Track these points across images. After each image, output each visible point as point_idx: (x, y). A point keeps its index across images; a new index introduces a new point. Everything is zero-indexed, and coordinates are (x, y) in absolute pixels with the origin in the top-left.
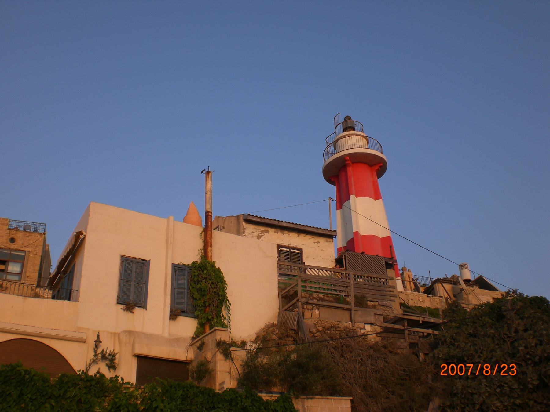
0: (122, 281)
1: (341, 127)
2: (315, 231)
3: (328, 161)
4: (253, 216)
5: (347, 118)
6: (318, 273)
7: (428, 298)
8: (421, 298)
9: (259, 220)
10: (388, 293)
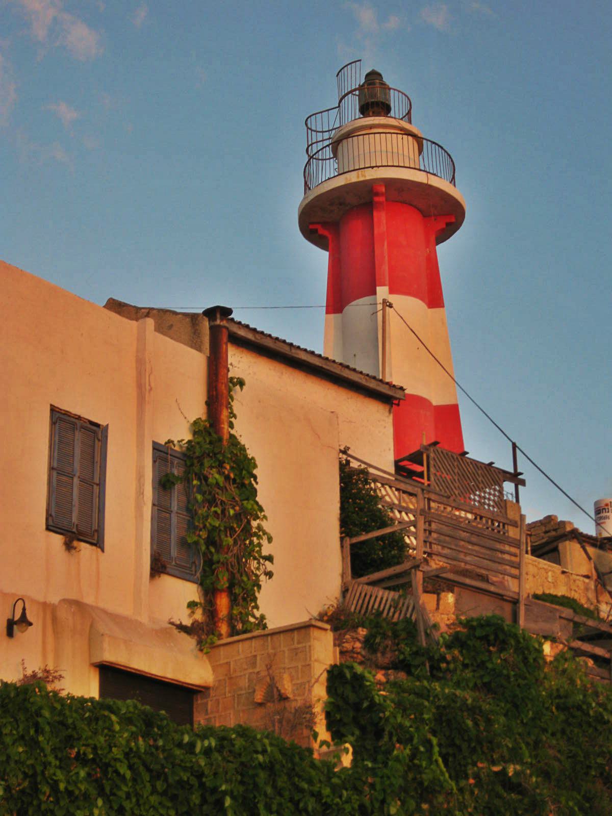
0: (55, 473)
1: (353, 104)
2: (363, 382)
3: (312, 195)
4: (240, 323)
5: (373, 77)
6: (399, 501)
7: (563, 576)
8: (550, 574)
9: (250, 336)
10: (507, 557)
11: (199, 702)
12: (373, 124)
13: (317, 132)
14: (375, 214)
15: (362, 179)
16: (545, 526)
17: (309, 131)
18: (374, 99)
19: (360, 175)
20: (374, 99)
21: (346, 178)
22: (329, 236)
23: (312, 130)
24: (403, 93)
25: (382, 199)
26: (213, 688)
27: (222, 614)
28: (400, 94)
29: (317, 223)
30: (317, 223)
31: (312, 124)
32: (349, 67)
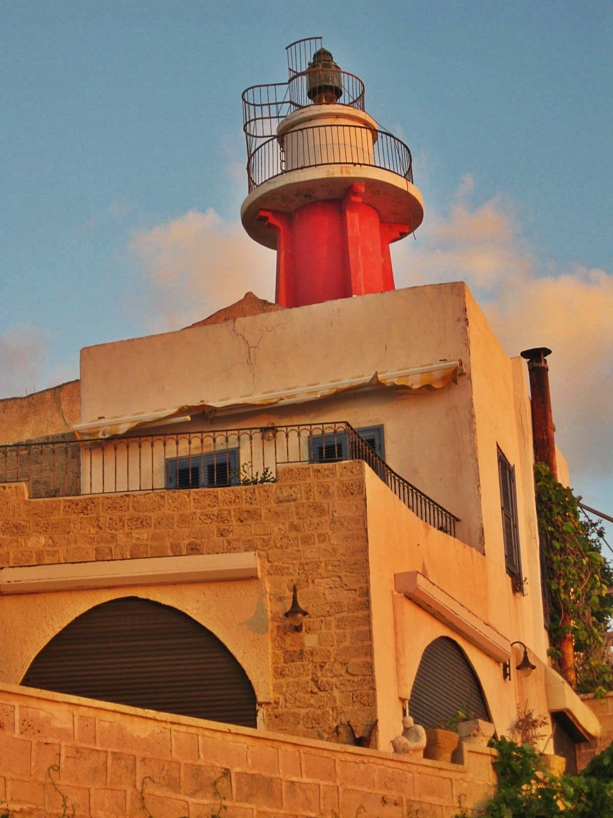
11: (583, 751)
12: (342, 114)
13: (255, 105)
14: (348, 214)
15: (345, 175)
16: (589, 637)
17: (247, 105)
18: (323, 84)
19: (344, 171)
20: (323, 84)
21: (328, 172)
22: (281, 227)
23: (250, 104)
24: (349, 74)
25: (359, 200)
26: (601, 740)
27: (570, 663)
28: (354, 79)
29: (269, 210)
30: (269, 210)
31: (249, 97)
32: (297, 45)
